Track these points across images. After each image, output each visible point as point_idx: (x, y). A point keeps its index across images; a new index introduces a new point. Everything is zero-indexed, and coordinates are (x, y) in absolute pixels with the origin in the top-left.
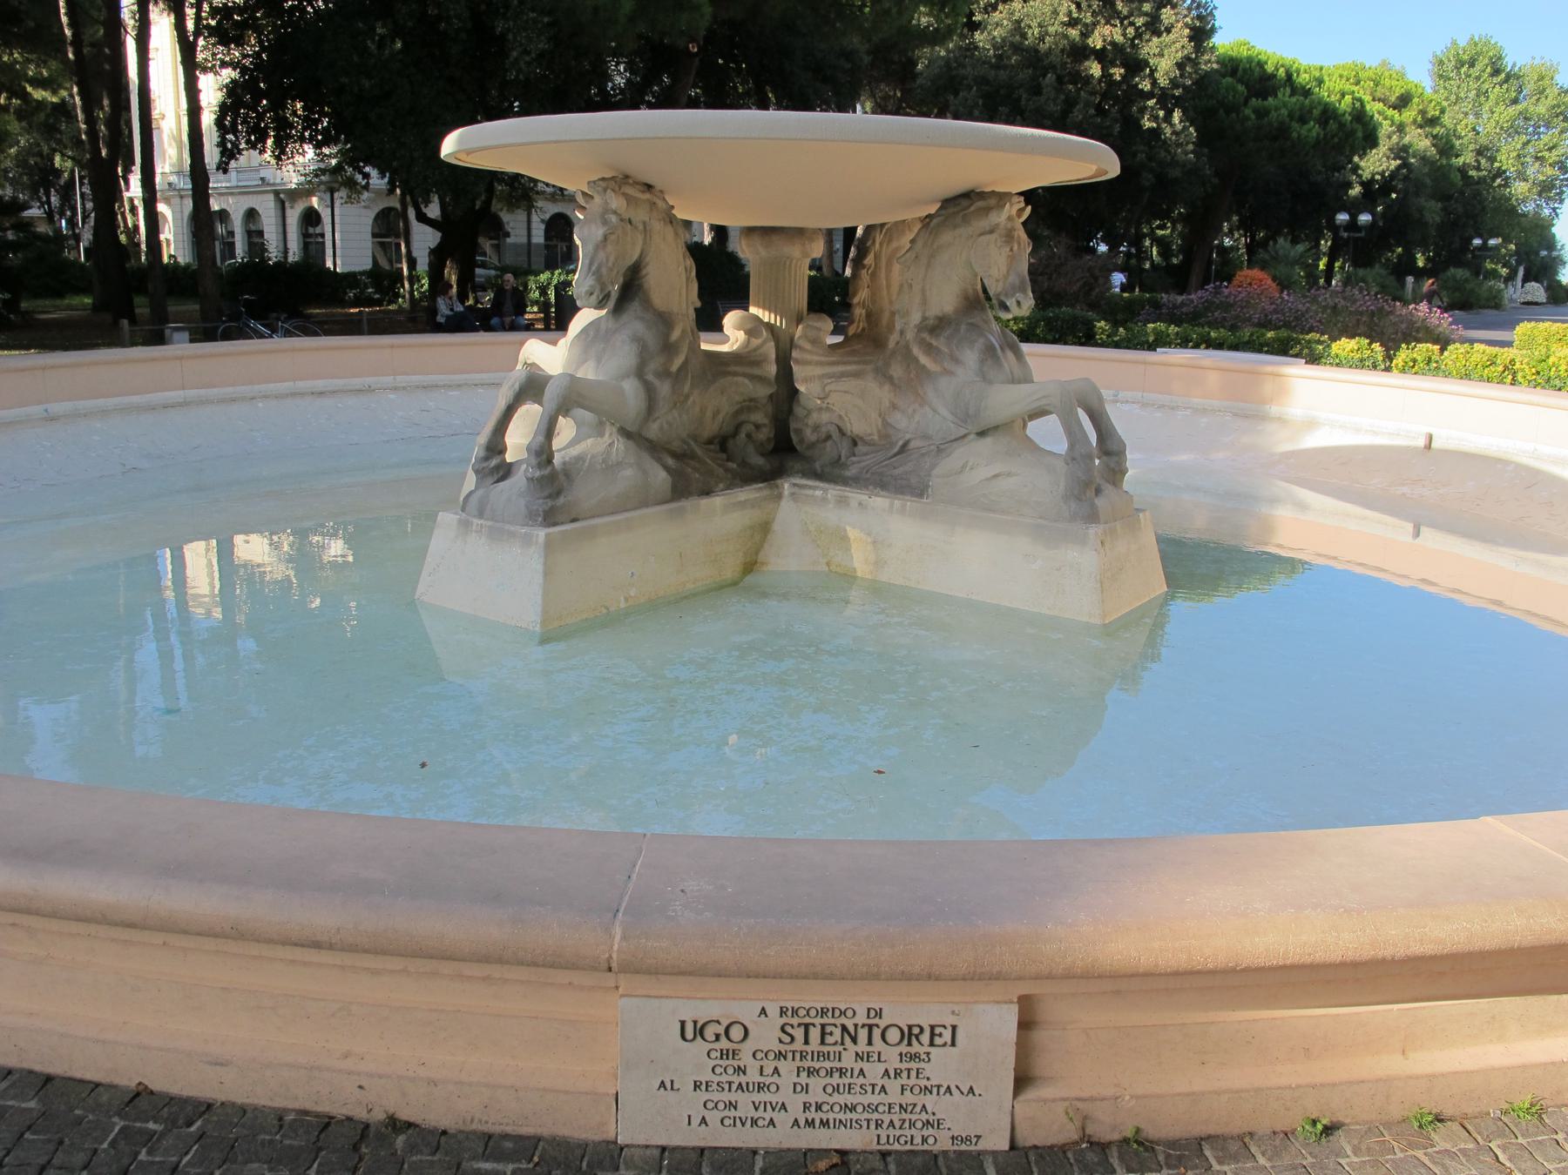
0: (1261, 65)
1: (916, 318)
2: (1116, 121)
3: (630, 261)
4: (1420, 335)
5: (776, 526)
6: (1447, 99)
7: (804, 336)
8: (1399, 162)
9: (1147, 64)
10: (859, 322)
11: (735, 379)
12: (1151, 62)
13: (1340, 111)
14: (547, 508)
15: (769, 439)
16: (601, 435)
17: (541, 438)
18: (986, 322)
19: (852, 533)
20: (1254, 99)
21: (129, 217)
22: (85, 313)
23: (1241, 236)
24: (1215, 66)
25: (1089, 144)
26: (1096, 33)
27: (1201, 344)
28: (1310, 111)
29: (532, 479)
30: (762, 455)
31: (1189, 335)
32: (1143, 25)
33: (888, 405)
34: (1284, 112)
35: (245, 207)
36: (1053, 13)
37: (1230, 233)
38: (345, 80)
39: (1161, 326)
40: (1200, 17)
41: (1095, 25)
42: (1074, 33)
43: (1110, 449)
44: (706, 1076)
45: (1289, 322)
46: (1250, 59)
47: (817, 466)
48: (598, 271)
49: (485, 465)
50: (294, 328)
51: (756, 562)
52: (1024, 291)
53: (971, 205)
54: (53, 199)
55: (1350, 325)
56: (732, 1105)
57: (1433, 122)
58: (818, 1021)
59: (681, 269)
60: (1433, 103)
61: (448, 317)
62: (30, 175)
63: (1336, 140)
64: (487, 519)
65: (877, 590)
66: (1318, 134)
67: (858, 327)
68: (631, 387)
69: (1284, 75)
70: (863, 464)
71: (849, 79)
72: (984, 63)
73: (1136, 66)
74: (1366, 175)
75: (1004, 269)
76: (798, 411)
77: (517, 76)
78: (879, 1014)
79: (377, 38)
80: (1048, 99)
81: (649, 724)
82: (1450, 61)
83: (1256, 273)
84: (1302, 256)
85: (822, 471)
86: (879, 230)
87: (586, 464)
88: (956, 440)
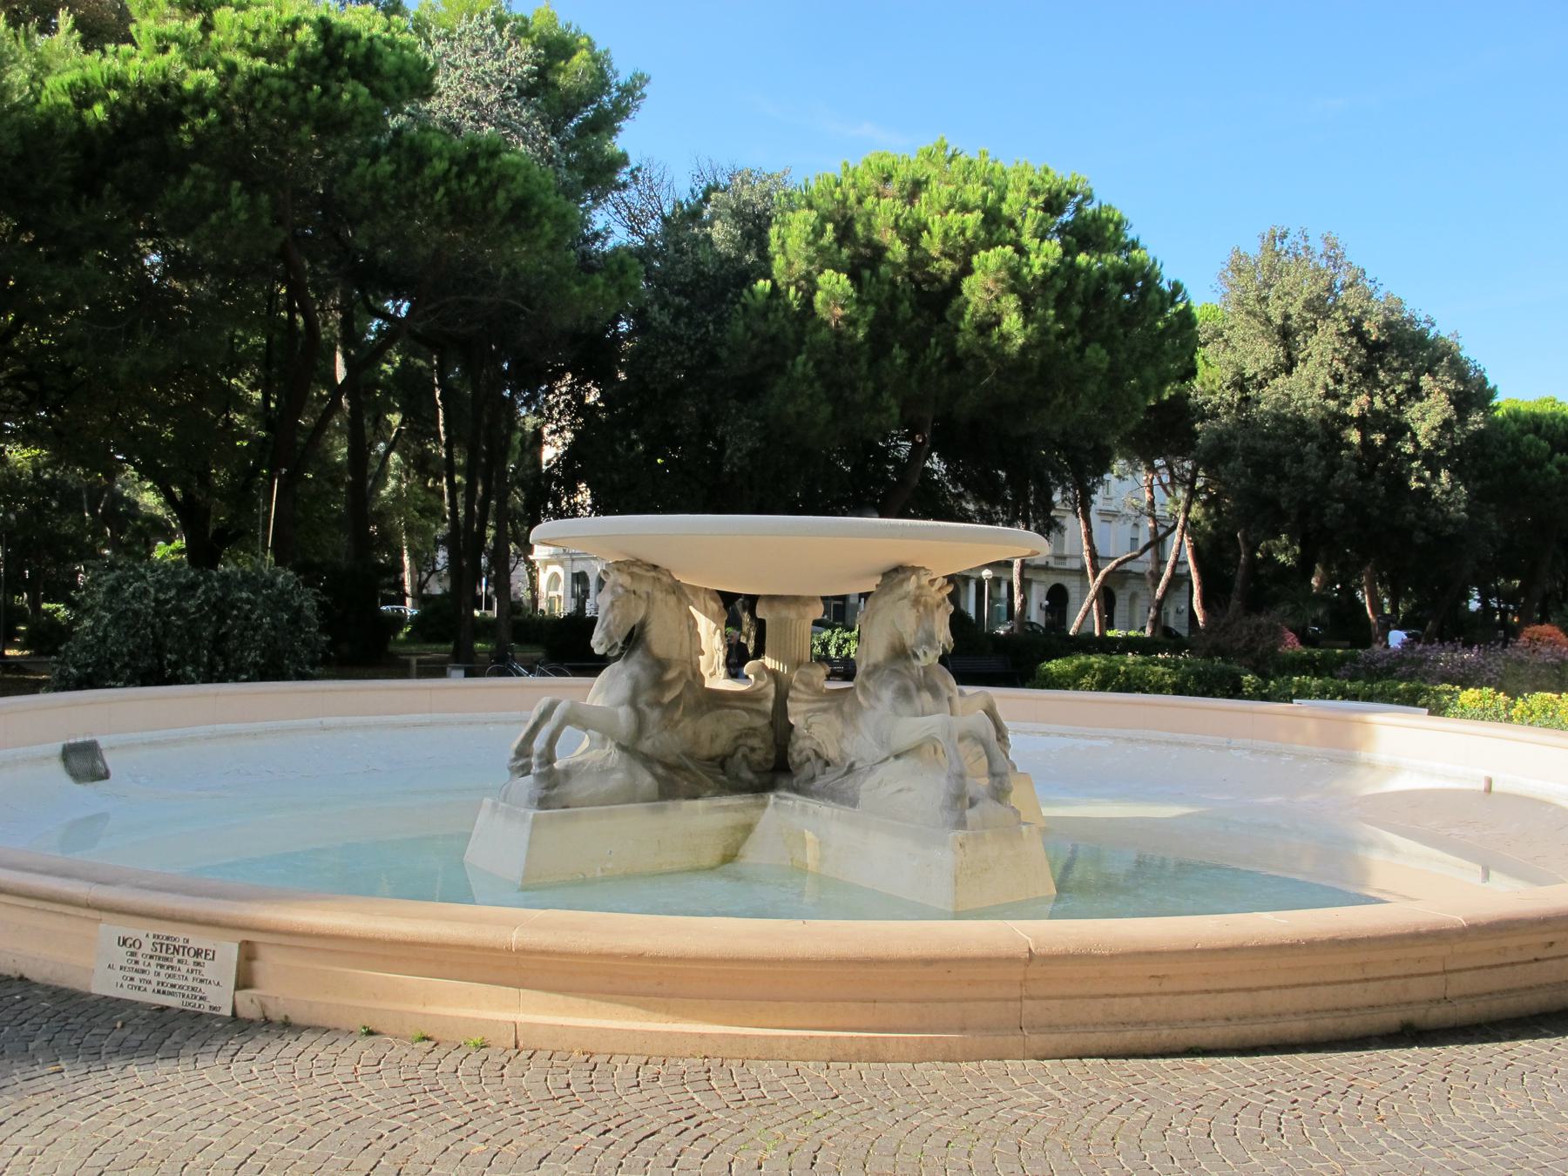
5: (758, 829)
9: (1410, 429)
11: (733, 711)
14: (542, 796)
19: (809, 835)
30: (755, 772)
44: (125, 964)
46: (1553, 416)
48: (608, 626)
50: (549, 670)
56: (132, 979)
58: (166, 942)
73: (1399, 430)
77: (731, 469)
78: (188, 941)
80: (1310, 466)
88: (882, 762)
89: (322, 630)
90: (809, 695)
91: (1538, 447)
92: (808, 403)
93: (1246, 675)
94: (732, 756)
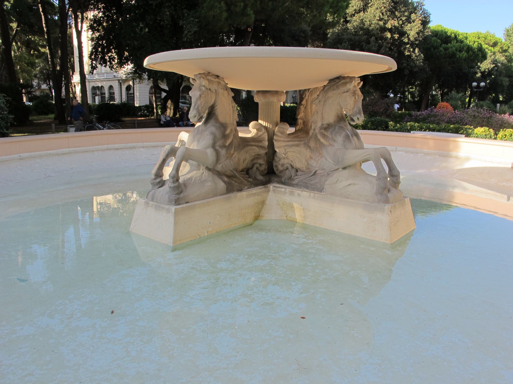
0: (446, 33)
1: (319, 124)
2: (396, 52)
3: (210, 104)
4: (506, 125)
5: (267, 202)
6: (510, 43)
7: (279, 131)
8: (494, 65)
9: (406, 33)
10: (300, 125)
11: (252, 147)
12: (408, 32)
13: (473, 48)
14: (176, 198)
15: (265, 169)
16: (199, 170)
17: (174, 172)
18: (346, 126)
19: (295, 205)
20: (443, 44)
21: (73, 88)
22: (52, 120)
23: (439, 91)
24: (430, 33)
25: (384, 57)
26: (389, 23)
27: (427, 130)
28: (463, 48)
29: (171, 187)
30: (262, 175)
31: (423, 127)
32: (405, 20)
33: (309, 157)
34: (454, 49)
35: (109, 85)
36: (374, 16)
37: (435, 90)
38: (129, 42)
39: (412, 123)
40: (425, 17)
41: (388, 20)
42: (381, 23)
43: (394, 173)
45: (458, 121)
46: (442, 31)
47: (283, 180)
48: (198, 108)
49: (155, 181)
51: (259, 216)
52: (360, 114)
53: (340, 82)
54: (51, 83)
55: (480, 122)
57: (505, 51)
59: (231, 107)
60: (505, 45)
61: (164, 122)
62: (44, 76)
63: (472, 58)
64: (154, 202)
65: (305, 227)
66: (466, 56)
67: (300, 126)
68: (210, 152)
69: (454, 36)
70: (301, 179)
71: (304, 40)
72: (351, 34)
73: (402, 34)
74: (482, 70)
75: (352, 106)
76: (276, 158)
77: (187, 40)
79: (139, 28)
81: (207, 290)
82: (511, 30)
83: (445, 104)
84: (461, 98)
85: (285, 181)
86: (307, 92)
87: (193, 181)
89: (10, 113)
90: (284, 138)
91: (437, 42)
92: (219, 11)
93: (390, 122)
94: (252, 167)
